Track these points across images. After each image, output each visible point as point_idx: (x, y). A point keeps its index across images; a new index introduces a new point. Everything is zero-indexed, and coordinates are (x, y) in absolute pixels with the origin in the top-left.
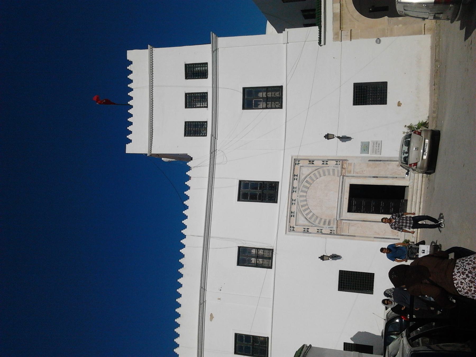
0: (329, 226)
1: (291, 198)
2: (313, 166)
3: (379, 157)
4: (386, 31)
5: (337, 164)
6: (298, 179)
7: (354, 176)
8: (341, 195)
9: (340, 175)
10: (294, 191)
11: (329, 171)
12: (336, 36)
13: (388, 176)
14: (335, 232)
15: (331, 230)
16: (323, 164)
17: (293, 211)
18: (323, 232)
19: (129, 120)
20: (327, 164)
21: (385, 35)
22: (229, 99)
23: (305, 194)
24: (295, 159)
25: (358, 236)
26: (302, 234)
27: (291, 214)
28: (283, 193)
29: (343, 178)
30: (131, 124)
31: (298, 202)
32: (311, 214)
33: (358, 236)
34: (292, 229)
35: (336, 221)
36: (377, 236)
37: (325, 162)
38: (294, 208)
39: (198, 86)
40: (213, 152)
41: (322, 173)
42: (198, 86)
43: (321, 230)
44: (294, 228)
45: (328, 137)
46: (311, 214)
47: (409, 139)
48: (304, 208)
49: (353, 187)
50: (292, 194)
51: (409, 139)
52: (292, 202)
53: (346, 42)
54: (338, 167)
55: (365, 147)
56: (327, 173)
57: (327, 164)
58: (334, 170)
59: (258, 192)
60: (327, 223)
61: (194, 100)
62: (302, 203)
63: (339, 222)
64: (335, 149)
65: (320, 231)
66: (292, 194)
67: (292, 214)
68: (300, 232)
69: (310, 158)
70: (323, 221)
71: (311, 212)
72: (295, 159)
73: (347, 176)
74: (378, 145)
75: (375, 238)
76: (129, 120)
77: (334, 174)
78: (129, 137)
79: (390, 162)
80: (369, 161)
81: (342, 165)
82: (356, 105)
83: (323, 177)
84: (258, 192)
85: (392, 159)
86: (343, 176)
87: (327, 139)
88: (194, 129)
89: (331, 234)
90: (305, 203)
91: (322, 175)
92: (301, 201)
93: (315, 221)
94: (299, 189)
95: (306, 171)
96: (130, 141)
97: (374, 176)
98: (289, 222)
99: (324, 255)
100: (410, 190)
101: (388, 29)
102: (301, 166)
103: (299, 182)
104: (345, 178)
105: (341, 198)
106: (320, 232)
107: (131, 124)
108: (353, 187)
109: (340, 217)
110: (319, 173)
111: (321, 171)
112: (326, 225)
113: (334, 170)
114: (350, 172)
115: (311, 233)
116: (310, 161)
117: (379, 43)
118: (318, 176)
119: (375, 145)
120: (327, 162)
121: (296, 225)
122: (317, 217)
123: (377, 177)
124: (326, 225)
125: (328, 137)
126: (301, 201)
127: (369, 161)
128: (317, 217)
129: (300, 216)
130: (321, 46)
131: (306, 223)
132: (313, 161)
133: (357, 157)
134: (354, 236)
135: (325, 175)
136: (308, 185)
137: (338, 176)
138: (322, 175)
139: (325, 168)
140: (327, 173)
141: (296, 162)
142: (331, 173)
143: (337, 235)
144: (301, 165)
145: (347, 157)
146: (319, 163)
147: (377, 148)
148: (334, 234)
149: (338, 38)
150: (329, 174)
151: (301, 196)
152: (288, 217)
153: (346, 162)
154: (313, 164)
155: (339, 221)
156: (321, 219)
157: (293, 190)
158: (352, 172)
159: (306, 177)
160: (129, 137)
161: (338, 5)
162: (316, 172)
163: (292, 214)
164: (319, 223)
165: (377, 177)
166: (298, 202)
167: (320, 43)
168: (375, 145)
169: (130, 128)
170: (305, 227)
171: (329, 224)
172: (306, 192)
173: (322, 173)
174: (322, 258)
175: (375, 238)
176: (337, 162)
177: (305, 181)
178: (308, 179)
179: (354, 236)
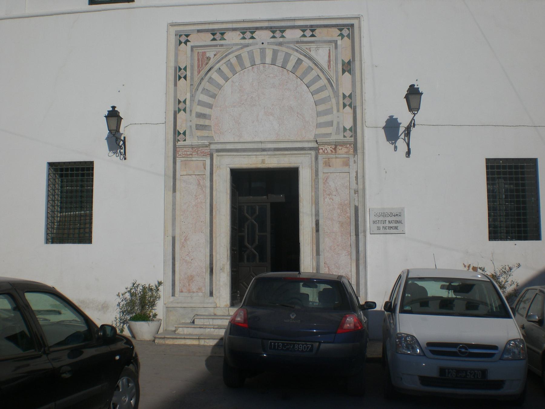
7: (317, 175)
16: (344, 96)
17: (225, 36)
18: (178, 116)
20: (344, 106)
25: (174, 197)
33: (174, 197)
38: (233, 38)
48: (234, 61)
58: (331, 124)
65: (182, 106)
68: (176, 61)
70: (206, 111)
73: (316, 158)
80: (356, 209)
83: (310, 99)
89: (177, 133)
94: (280, 44)
110: (322, 89)
111: (328, 92)
121: (192, 47)
127: (356, 209)
139: (334, 101)
144: (339, 42)
147: (387, 224)
150: (319, 114)
154: (344, 72)
158: (327, 170)
162: (323, 81)
178: (307, 62)
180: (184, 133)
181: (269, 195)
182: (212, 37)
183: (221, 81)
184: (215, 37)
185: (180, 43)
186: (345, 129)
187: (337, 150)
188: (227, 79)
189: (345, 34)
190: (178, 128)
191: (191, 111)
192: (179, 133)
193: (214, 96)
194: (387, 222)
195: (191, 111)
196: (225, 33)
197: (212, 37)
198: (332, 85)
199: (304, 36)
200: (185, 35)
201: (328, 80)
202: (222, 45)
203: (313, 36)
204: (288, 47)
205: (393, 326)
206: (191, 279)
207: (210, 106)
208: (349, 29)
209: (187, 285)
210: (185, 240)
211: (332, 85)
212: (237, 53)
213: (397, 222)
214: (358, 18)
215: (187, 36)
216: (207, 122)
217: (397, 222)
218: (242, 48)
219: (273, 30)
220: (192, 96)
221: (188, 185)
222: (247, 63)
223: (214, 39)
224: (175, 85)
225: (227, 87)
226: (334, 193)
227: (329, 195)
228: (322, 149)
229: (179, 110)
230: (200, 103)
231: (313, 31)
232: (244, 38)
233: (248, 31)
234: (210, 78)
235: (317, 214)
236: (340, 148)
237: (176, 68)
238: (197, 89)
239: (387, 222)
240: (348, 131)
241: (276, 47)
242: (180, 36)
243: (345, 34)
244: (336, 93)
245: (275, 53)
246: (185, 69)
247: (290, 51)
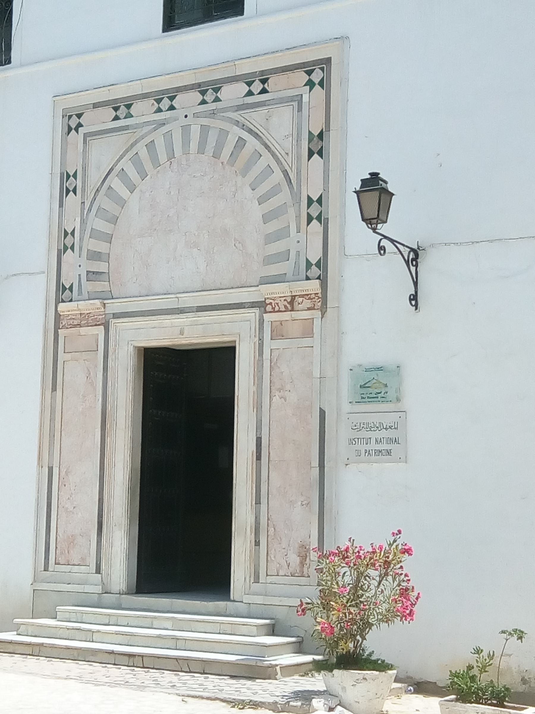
2: (299, 158)
5: (309, 264)
6: (250, 100)
7: (261, 353)
11: (282, 234)
13: (263, 507)
16: (310, 201)
17: (133, 111)
18: (64, 257)
20: (310, 219)
25: (53, 399)
32: (124, 192)
33: (53, 399)
38: (143, 111)
41: (274, 202)
47: (278, 668)
48: (143, 153)
49: (221, 358)
51: (278, 668)
55: (376, 386)
56: (273, 226)
58: (285, 256)
65: (69, 241)
68: (63, 163)
70: (101, 247)
73: (261, 322)
74: (388, 445)
80: (322, 413)
83: (257, 212)
89: (61, 288)
94: (213, 114)
95: (281, 126)
100: (221, 604)
110: (275, 191)
111: (284, 196)
121: (85, 135)
127: (322, 413)
129: (118, 142)
131: (95, 177)
133: (338, 352)
139: (292, 212)
144: (305, 98)
147: (373, 446)
150: (269, 239)
154: (311, 154)
158: (278, 344)
162: (278, 175)
163: (122, 112)
168: (384, 434)
173: (274, 202)
178: (252, 142)
180: (71, 289)
181: (318, 468)
182: (114, 114)
183: (124, 192)
184: (118, 113)
185: (70, 129)
186: (309, 264)
187: (296, 304)
188: (132, 189)
189: (317, 81)
190: (63, 280)
191: (81, 249)
192: (64, 289)
193: (114, 220)
194: (373, 441)
195: (81, 249)
196: (132, 104)
197: (114, 114)
198: (289, 181)
199: (250, 93)
200: (77, 115)
201: (285, 173)
202: (126, 128)
203: (264, 91)
204: (224, 119)
205: (136, 381)
206: (71, 541)
207: (109, 238)
208: (322, 69)
209: (66, 552)
210: (67, 473)
211: (289, 181)
212: (148, 140)
213: (391, 441)
214: (344, 39)
215: (79, 116)
216: (102, 267)
217: (391, 441)
218: (155, 129)
219: (202, 88)
220: (83, 222)
221: (77, 373)
222: (163, 157)
223: (116, 118)
224: (61, 205)
225: (134, 201)
226: (288, 387)
227: (279, 390)
228: (271, 304)
229: (66, 248)
230: (95, 234)
231: (264, 81)
232: (159, 110)
233: (164, 99)
234: (110, 188)
235: (259, 427)
236: (300, 300)
237: (62, 175)
238: (90, 210)
239: (373, 441)
240: (314, 267)
241: (205, 121)
242: (70, 117)
243: (317, 81)
244: (296, 196)
245: (205, 129)
246: (75, 176)
247: (226, 126)
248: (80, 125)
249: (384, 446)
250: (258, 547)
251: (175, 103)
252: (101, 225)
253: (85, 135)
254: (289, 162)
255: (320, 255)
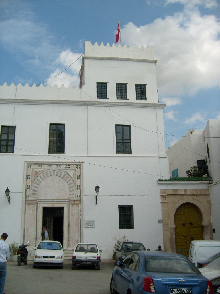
0: (32, 194)
1: (52, 164)
3: (83, 227)
4: (166, 227)
5: (78, 196)
7: (69, 209)
8: (55, 202)
9: (70, 199)
10: (57, 166)
12: (163, 192)
13: (70, 235)
14: (28, 199)
15: (29, 196)
16: (78, 186)
17: (43, 166)
18: (27, 190)
19: (108, 44)
20: (78, 189)
21: (164, 225)
22: (124, 115)
23: (55, 174)
24: (81, 164)
25: (25, 216)
26: (25, 174)
27: (40, 165)
28: (56, 158)
29: (68, 202)
30: (105, 45)
31: (49, 169)
32: (41, 180)
33: (25, 216)
34: (29, 166)
35: (36, 199)
36: (25, 231)
37: (79, 187)
39: (131, 92)
40: (85, 104)
41: (72, 185)
42: (131, 92)
43: (29, 189)
44: (30, 167)
45: (97, 188)
46: (41, 180)
48: (45, 174)
50: (55, 164)
52: (50, 165)
53: (159, 199)
54: (76, 197)
56: (71, 189)
57: (78, 189)
58: (73, 194)
59: (57, 139)
60: (34, 192)
61: (122, 89)
62: (48, 172)
63: (36, 201)
64: (89, 190)
65: (28, 187)
66: (55, 164)
67: (40, 166)
68: (27, 173)
69: (82, 176)
70: (36, 189)
71: (43, 179)
72: (81, 164)
73: (69, 204)
75: (24, 229)
76: (108, 44)
77: (70, 195)
78: (96, 44)
79: (80, 234)
81: (77, 200)
82: (119, 207)
83: (67, 186)
84: (57, 139)
85: (82, 236)
86: (69, 202)
87: (95, 187)
88: (102, 90)
89: (26, 196)
90: (49, 175)
91: (70, 186)
92: (50, 172)
93: (36, 183)
94: (59, 169)
96: (93, 44)
97: (70, 224)
98: (34, 164)
99: (9, 191)
101: (167, 228)
102: (76, 169)
103: (64, 169)
104: (68, 203)
105: (53, 202)
106: (28, 187)
107: (105, 45)
108: (62, 209)
109: (39, 202)
112: (32, 192)
113: (73, 194)
114: (72, 206)
115: (26, 180)
116: (79, 176)
117: (159, 222)
118: (69, 183)
119: (91, 223)
120: (79, 189)
121: (32, 169)
122: (38, 185)
123: (69, 226)
124: (32, 192)
125: (97, 188)
126: (50, 172)
128: (38, 185)
130: (158, 181)
132: (79, 179)
134: (25, 214)
135: (69, 188)
136: (62, 176)
137: (69, 198)
138: (70, 186)
139: (75, 187)
140: (71, 189)
141: (79, 165)
142: (71, 193)
143: (26, 200)
144: (77, 170)
145: (83, 203)
146: (78, 182)
147: (90, 225)
148: (26, 198)
149: (163, 193)
150: (70, 191)
151: (54, 171)
152: (38, 163)
153: (80, 202)
154: (78, 178)
155: (36, 201)
156: (37, 188)
157: (58, 165)
158: (72, 208)
159: (68, 174)
160: (96, 44)
161: (183, 193)
162: (72, 181)
163: (40, 166)
164: (34, 187)
165: (69, 226)
166: (49, 169)
167: (160, 180)
169: (102, 44)
170: (31, 176)
171: (34, 194)
172: (57, 175)
173: (72, 185)
174: (7, 191)
175: (24, 229)
176: (79, 196)
177: (66, 174)
178: (67, 175)
179: (25, 214)
190: (27, 194)
191: (31, 189)
195: (31, 189)
213: (92, 224)
215: (31, 165)
217: (92, 224)
218: (47, 170)
219: (57, 165)
221: (29, 212)
225: (43, 182)
226: (74, 215)
243: (79, 167)
246: (30, 176)
248: (31, 167)
249: (92, 225)
250: (187, 190)
251: (51, 166)
252: (35, 185)
253: (32, 169)
254: (74, 179)
255: (80, 194)
